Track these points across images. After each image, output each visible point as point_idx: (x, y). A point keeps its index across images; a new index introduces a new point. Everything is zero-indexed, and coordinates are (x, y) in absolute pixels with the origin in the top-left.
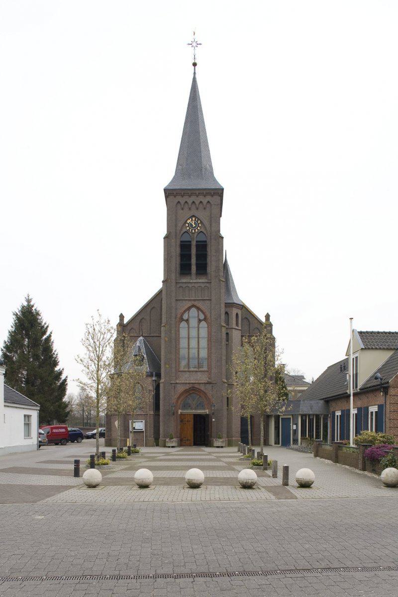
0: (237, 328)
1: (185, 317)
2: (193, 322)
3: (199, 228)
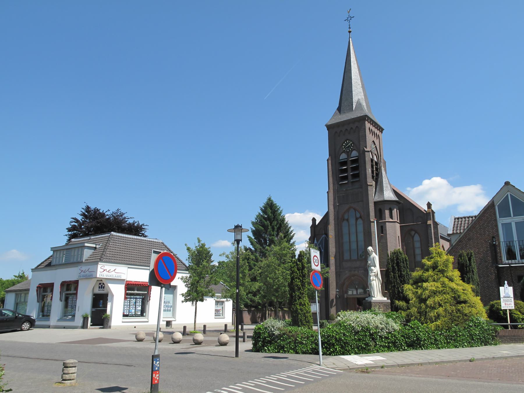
0: (391, 220)
1: (346, 217)
2: (352, 221)
3: (352, 147)
